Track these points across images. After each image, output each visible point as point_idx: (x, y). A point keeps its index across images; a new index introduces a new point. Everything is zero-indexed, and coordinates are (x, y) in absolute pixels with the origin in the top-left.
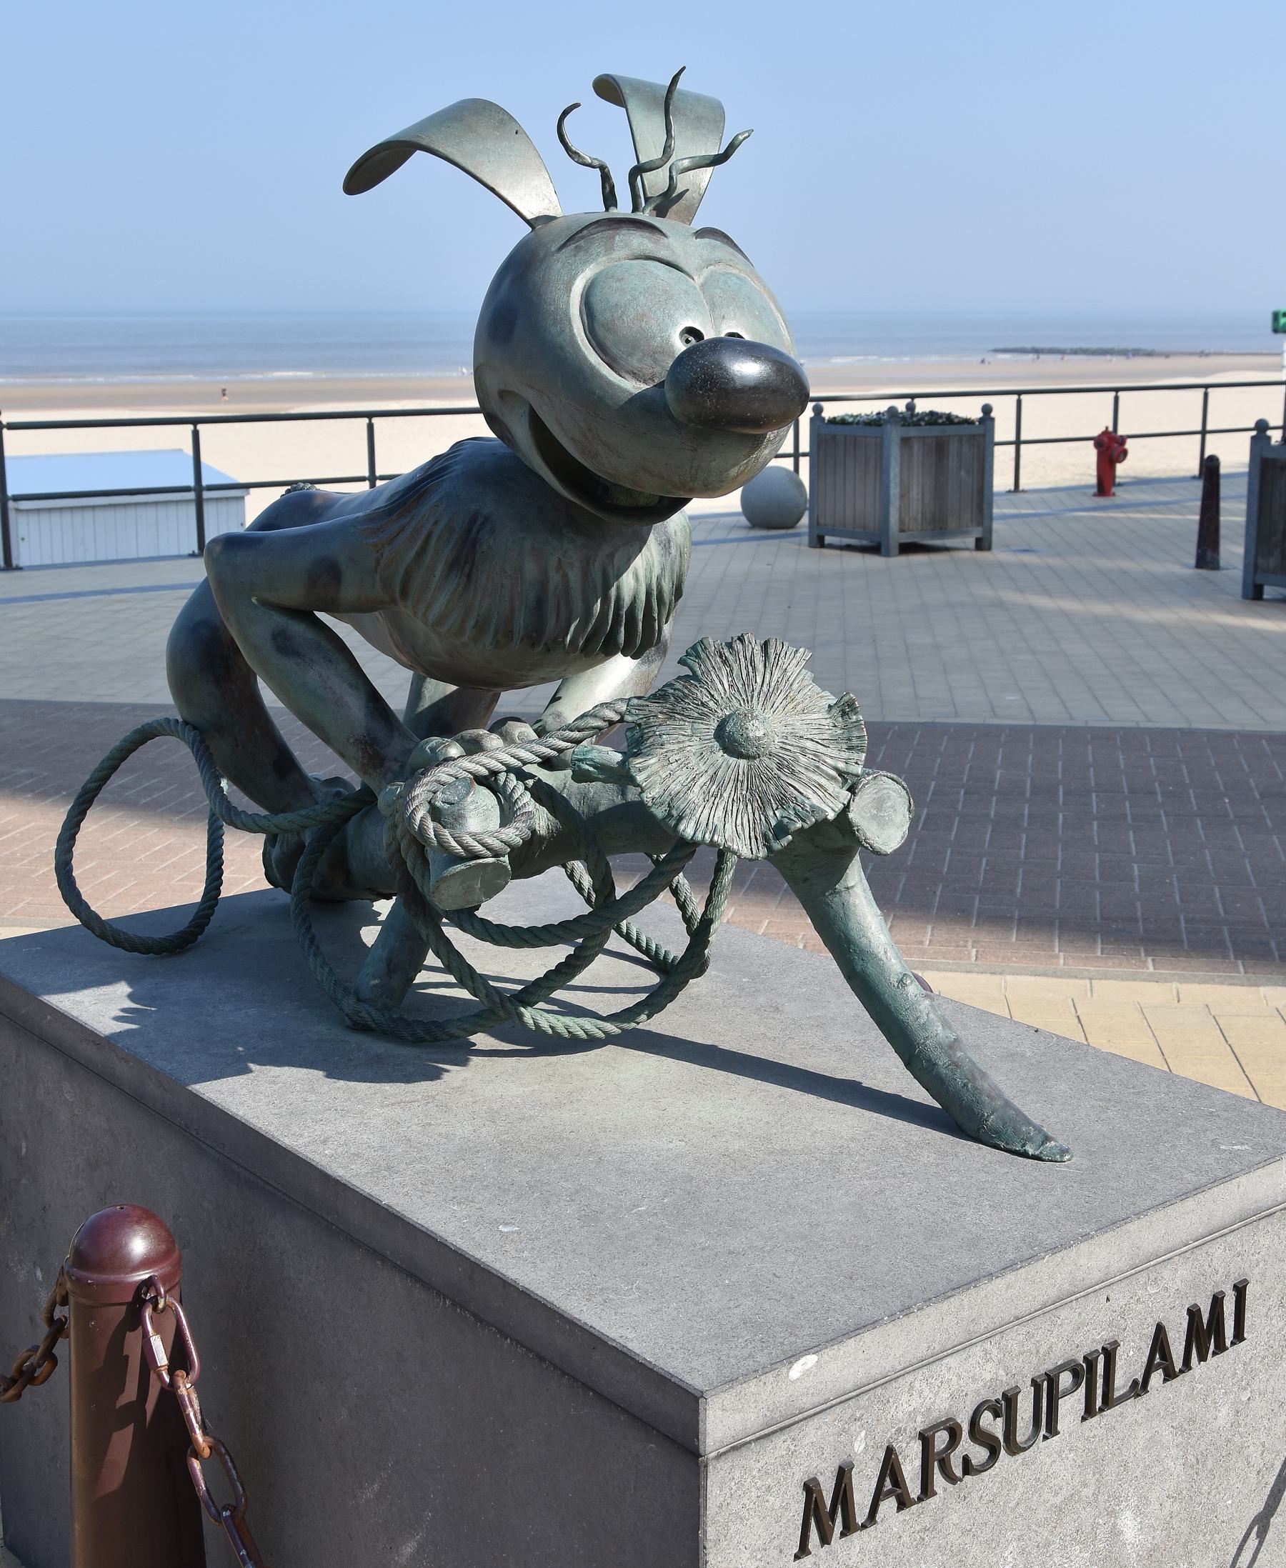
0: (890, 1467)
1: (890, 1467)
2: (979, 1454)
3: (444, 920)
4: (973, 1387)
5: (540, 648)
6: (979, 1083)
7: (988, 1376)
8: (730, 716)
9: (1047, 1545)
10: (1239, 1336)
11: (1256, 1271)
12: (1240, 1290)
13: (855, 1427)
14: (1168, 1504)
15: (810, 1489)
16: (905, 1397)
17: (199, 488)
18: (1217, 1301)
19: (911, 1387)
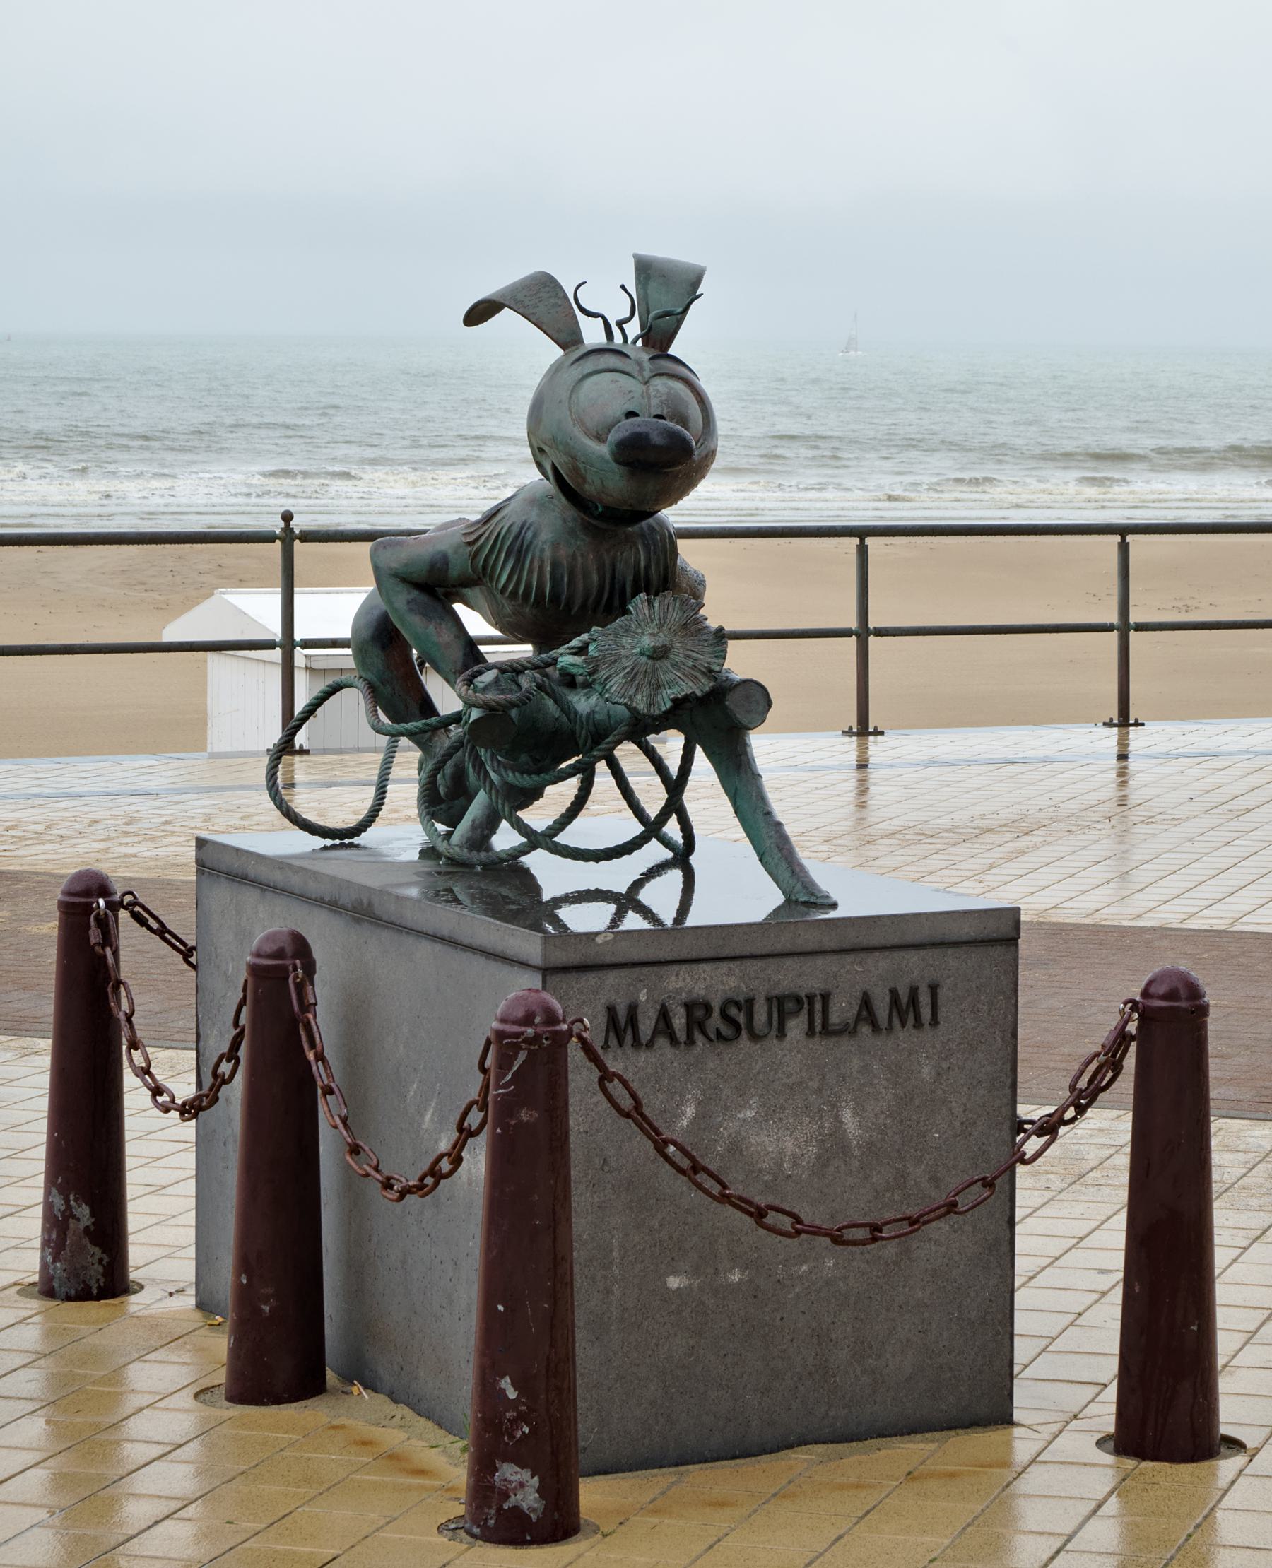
0: (664, 1015)
1: (664, 1015)
2: (726, 1031)
3: (414, 892)
4: (721, 987)
5: (493, 1038)
6: (571, 443)
7: (733, 985)
8: (592, 749)
9: (783, 1108)
10: (935, 1022)
11: (948, 981)
12: (934, 989)
13: (639, 985)
14: (882, 1117)
15: (611, 1010)
16: (673, 978)
17: (288, 644)
18: (914, 992)
19: (677, 975)
